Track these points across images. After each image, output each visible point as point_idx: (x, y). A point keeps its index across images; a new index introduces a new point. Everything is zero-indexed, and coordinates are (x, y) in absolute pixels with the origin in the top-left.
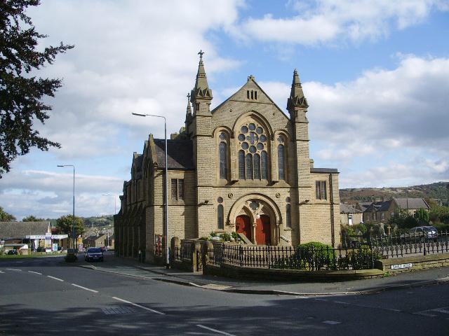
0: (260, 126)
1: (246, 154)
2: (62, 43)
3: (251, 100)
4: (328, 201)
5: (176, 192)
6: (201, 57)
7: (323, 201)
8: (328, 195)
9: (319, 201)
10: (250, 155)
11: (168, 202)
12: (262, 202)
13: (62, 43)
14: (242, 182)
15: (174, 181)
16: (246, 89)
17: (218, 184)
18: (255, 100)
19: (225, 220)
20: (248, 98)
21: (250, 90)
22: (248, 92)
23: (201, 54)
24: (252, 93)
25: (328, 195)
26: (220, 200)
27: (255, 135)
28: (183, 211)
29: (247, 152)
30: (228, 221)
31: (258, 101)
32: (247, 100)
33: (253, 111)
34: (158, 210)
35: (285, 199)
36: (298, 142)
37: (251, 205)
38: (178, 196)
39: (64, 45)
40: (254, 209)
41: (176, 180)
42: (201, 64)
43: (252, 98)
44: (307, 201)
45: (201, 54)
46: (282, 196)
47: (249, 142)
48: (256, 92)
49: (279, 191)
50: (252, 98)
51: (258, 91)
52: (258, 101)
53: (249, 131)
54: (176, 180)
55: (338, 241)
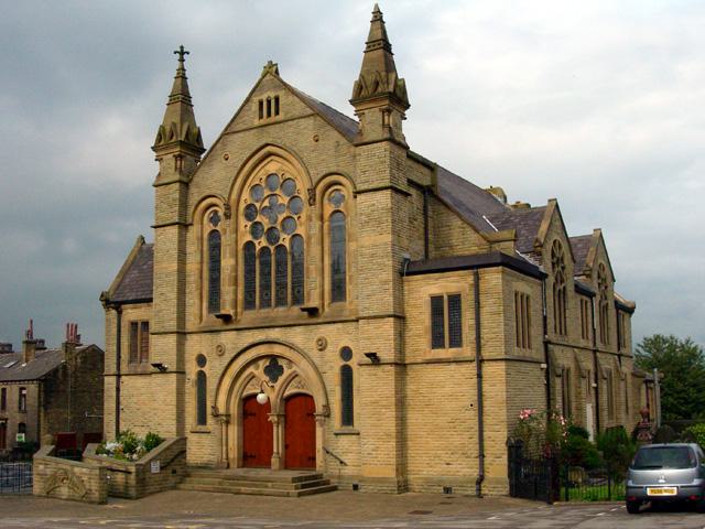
1: (258, 248)
2: (188, 53)
4: (467, 350)
6: (182, 60)
10: (265, 250)
13: (188, 53)
14: (248, 317)
16: (256, 99)
18: (274, 118)
19: (209, 410)
21: (264, 97)
22: (261, 103)
23: (182, 53)
24: (269, 102)
25: (468, 334)
26: (201, 360)
29: (262, 242)
30: (215, 407)
31: (281, 116)
32: (257, 122)
33: (267, 145)
34: (110, 382)
36: (106, 378)
39: (185, 56)
41: (136, 324)
42: (182, 76)
45: (182, 53)
46: (329, 348)
48: (277, 99)
50: (269, 115)
51: (281, 94)
52: (281, 116)
54: (136, 324)
55: (498, 467)
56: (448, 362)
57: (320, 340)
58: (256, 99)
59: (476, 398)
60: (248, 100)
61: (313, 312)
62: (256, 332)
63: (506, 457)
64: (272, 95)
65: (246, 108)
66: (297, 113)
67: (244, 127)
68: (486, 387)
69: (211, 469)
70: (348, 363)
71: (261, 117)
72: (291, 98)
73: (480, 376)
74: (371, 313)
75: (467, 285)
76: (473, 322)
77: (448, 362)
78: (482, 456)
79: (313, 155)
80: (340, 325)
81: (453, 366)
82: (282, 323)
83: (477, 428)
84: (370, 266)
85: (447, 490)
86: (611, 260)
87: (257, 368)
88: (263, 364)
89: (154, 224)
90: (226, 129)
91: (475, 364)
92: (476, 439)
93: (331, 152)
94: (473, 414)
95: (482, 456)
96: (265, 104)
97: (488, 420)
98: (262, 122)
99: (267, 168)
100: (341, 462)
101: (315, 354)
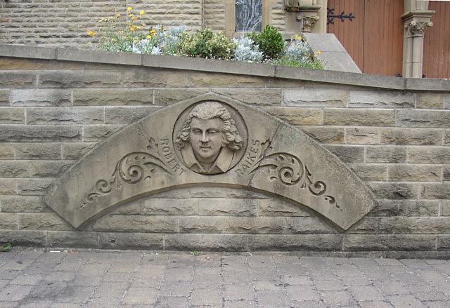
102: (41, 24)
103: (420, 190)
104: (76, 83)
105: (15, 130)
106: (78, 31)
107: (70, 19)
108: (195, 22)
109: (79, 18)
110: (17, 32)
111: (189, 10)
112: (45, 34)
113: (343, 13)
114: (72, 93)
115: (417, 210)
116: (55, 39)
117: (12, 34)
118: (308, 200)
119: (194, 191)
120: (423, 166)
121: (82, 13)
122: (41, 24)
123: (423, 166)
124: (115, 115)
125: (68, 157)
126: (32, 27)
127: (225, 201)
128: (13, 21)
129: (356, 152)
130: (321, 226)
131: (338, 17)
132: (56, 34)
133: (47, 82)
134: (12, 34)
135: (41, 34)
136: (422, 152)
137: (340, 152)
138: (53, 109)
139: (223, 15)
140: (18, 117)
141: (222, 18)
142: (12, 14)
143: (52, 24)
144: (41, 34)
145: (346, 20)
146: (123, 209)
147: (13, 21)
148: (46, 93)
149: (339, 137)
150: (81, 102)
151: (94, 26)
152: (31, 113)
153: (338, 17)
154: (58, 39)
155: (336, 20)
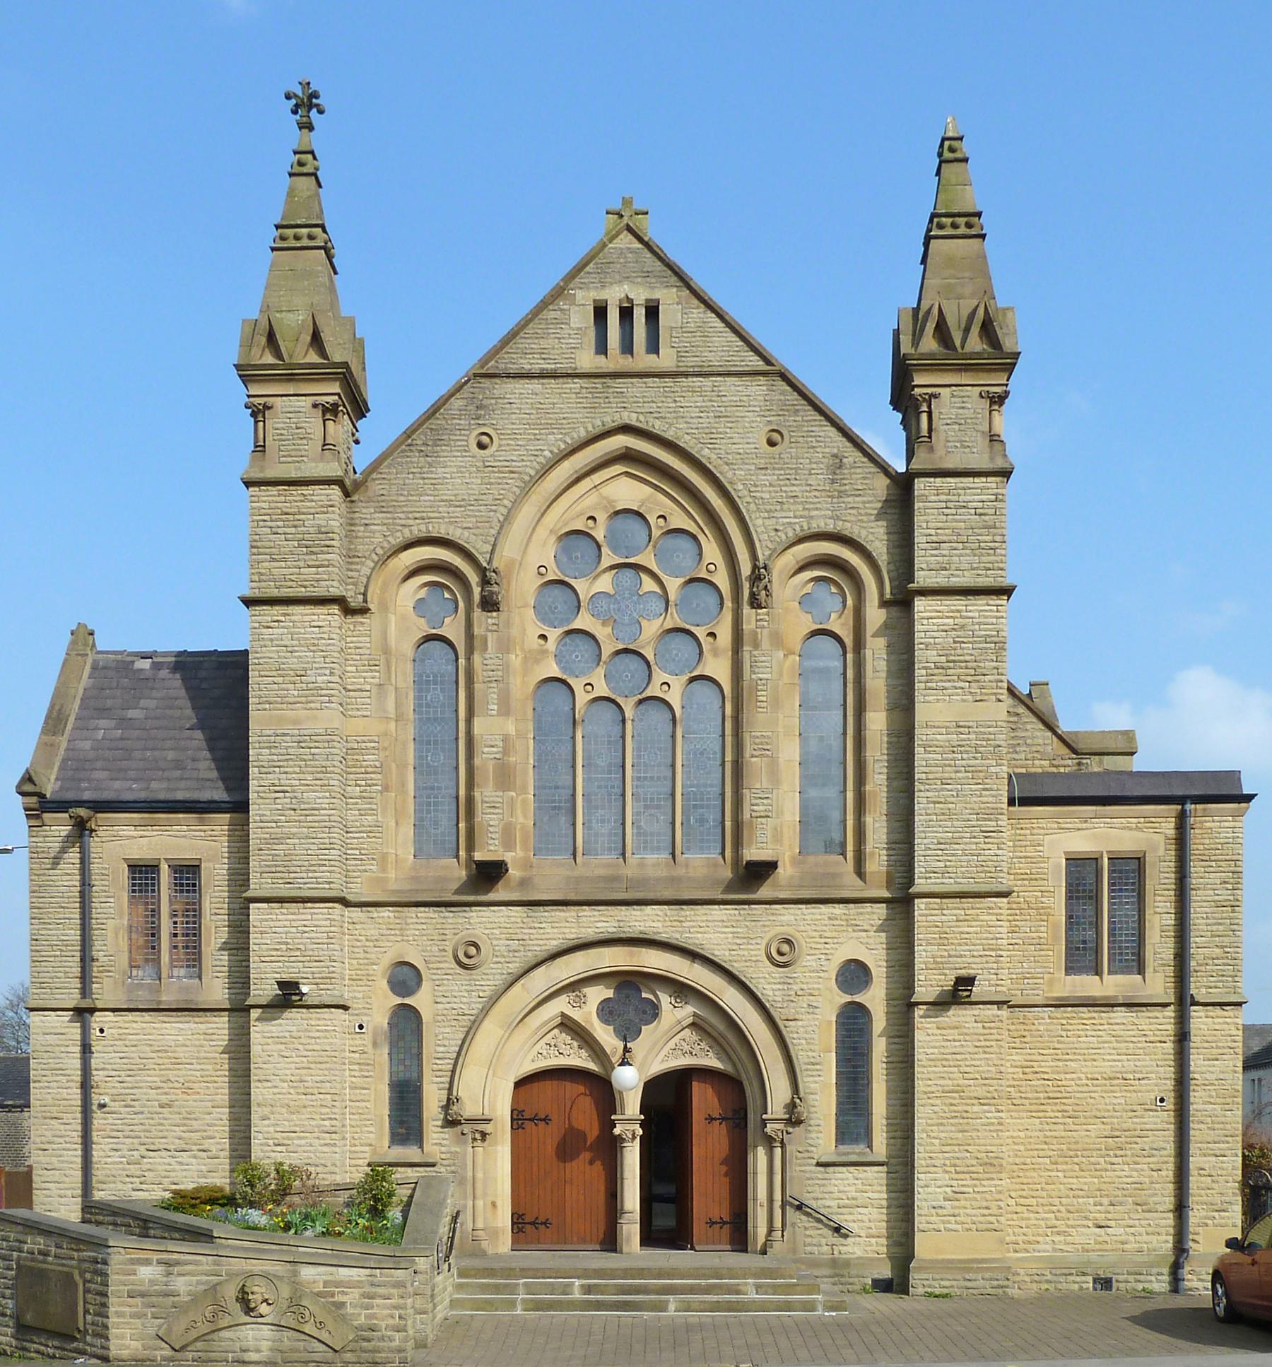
0: (679, 520)
2: (321, 112)
3: (615, 360)
4: (1158, 983)
5: (154, 934)
7: (1112, 984)
8: (1159, 946)
9: (1088, 985)
11: (106, 991)
12: (682, 990)
15: (143, 874)
16: (585, 297)
17: (396, 881)
18: (643, 360)
19: (433, 1098)
20: (602, 348)
21: (614, 295)
22: (600, 312)
24: (626, 313)
25: (1159, 946)
27: (648, 584)
28: (899, 471)
32: (587, 360)
33: (626, 429)
35: (833, 968)
37: (607, 1011)
38: (165, 958)
40: (628, 1033)
43: (627, 347)
44: (966, 982)
45: (357, 442)
46: (807, 961)
47: (601, 632)
48: (652, 312)
49: (789, 919)
50: (627, 347)
52: (666, 359)
53: (609, 558)
56: (1109, 1004)
57: (788, 942)
58: (585, 297)
59: (1170, 1084)
60: (558, 293)
61: (759, 872)
62: (570, 913)
63: (1238, 1208)
64: (640, 296)
65: (550, 315)
66: (715, 359)
67: (538, 365)
68: (1196, 1062)
69: (260, 1229)
70: (858, 998)
71: (602, 348)
72: (698, 313)
73: (1182, 1037)
74: (950, 885)
75: (1160, 839)
76: (1170, 920)
77: (1109, 1004)
78: (1181, 1208)
79: (764, 478)
80: (838, 910)
81: (1120, 1014)
82: (668, 894)
83: (1170, 1148)
84: (949, 773)
85: (1105, 1283)
86: (60, 666)
87: (580, 1002)
88: (597, 994)
89: (248, 593)
90: (484, 361)
91: (1170, 1012)
92: (1169, 1172)
93: (820, 479)
94: (1165, 1118)
95: (1181, 1208)
96: (639, 315)
97: (1197, 1132)
98: (602, 363)
99: (607, 490)
100: (837, 1230)
101: (766, 981)
102: (147, 1134)
103: (384, 1326)
104: (178, 1263)
105: (139, 1291)
106: (196, 1144)
107: (185, 1128)
108: (332, 1142)
109: (197, 1128)
110: (117, 1143)
111: (325, 1129)
112: (152, 1147)
113: (536, 1115)
114: (176, 1269)
115: (382, 1339)
116: (164, 1153)
117: (111, 1146)
118: (315, 1333)
119: (248, 1326)
120: (386, 1312)
121: (199, 1122)
122: (147, 1134)
123: (386, 1312)
124: (198, 1283)
125: (28, 1252)
126: (137, 1137)
127: (266, 1331)
128: (113, 1130)
129: (343, 1304)
130: (327, 1349)
131: (529, 1120)
132: (166, 1146)
133: (159, 1262)
134: (111, 1146)
135: (147, 1147)
136: (384, 1304)
137: (334, 1304)
138: (165, 1279)
139: (372, 1129)
140: (142, 1282)
141: (371, 1132)
142: (110, 1121)
143: (160, 1134)
144: (147, 1147)
145: (542, 1124)
146: (206, 1338)
147: (113, 1130)
148: (161, 1269)
149: (333, 1295)
150: (180, 1275)
151: (214, 1138)
152: (149, 1281)
153: (529, 1120)
154: (169, 1153)
155: (528, 1124)
